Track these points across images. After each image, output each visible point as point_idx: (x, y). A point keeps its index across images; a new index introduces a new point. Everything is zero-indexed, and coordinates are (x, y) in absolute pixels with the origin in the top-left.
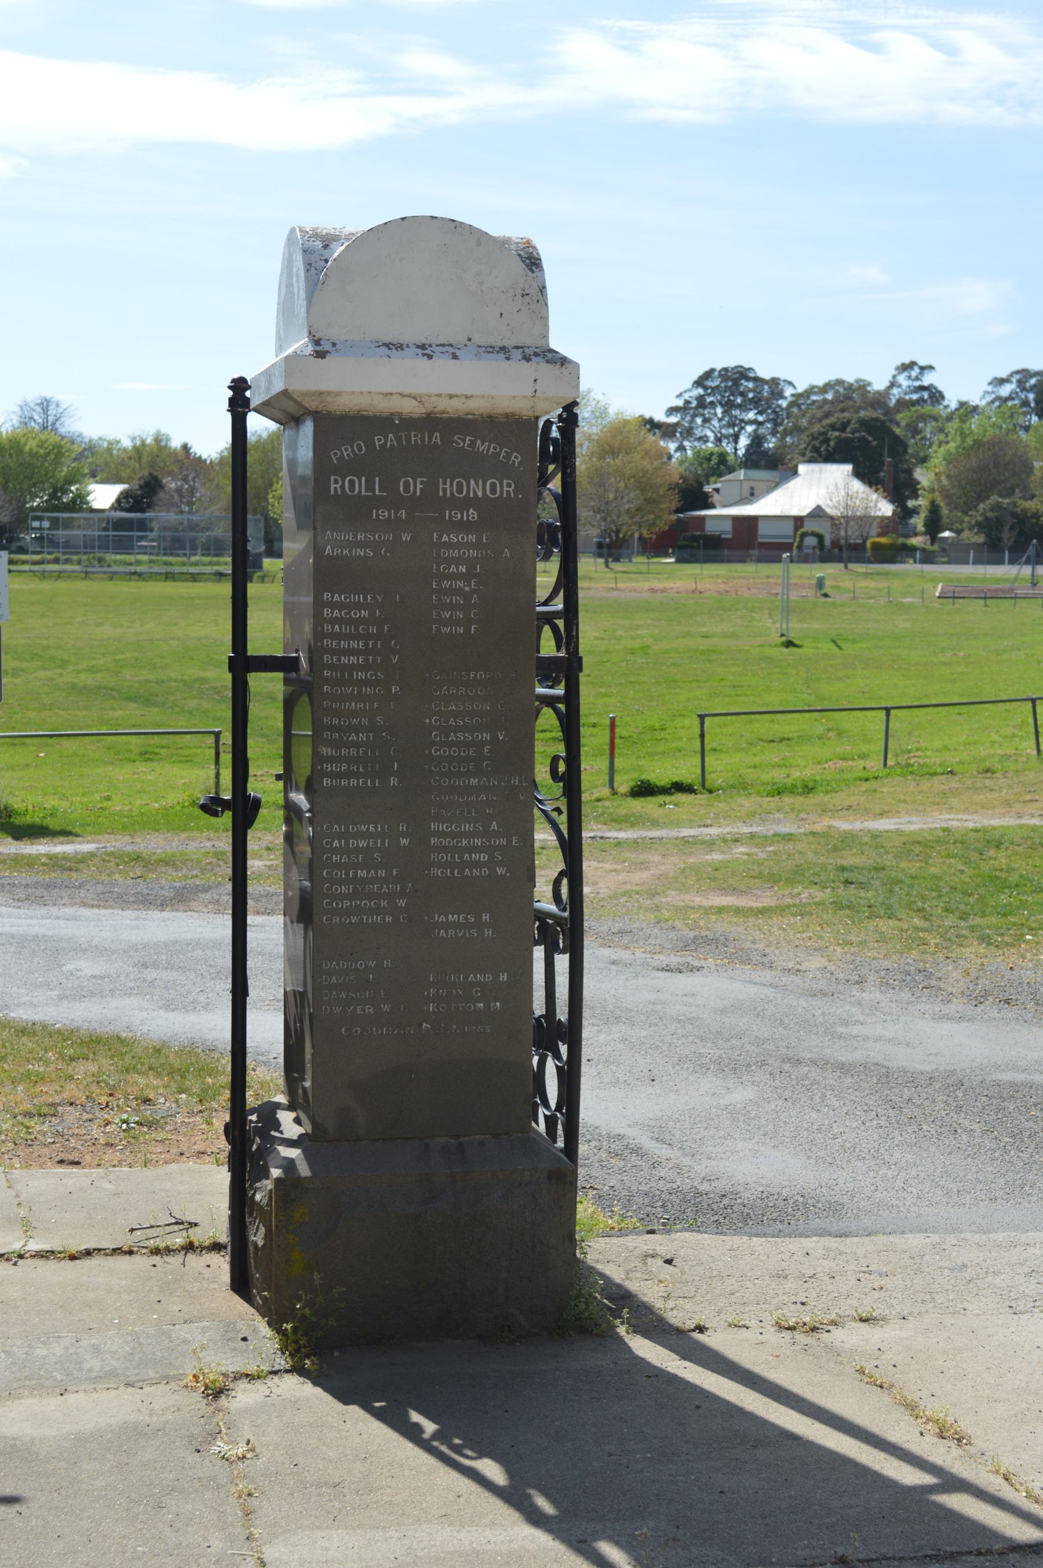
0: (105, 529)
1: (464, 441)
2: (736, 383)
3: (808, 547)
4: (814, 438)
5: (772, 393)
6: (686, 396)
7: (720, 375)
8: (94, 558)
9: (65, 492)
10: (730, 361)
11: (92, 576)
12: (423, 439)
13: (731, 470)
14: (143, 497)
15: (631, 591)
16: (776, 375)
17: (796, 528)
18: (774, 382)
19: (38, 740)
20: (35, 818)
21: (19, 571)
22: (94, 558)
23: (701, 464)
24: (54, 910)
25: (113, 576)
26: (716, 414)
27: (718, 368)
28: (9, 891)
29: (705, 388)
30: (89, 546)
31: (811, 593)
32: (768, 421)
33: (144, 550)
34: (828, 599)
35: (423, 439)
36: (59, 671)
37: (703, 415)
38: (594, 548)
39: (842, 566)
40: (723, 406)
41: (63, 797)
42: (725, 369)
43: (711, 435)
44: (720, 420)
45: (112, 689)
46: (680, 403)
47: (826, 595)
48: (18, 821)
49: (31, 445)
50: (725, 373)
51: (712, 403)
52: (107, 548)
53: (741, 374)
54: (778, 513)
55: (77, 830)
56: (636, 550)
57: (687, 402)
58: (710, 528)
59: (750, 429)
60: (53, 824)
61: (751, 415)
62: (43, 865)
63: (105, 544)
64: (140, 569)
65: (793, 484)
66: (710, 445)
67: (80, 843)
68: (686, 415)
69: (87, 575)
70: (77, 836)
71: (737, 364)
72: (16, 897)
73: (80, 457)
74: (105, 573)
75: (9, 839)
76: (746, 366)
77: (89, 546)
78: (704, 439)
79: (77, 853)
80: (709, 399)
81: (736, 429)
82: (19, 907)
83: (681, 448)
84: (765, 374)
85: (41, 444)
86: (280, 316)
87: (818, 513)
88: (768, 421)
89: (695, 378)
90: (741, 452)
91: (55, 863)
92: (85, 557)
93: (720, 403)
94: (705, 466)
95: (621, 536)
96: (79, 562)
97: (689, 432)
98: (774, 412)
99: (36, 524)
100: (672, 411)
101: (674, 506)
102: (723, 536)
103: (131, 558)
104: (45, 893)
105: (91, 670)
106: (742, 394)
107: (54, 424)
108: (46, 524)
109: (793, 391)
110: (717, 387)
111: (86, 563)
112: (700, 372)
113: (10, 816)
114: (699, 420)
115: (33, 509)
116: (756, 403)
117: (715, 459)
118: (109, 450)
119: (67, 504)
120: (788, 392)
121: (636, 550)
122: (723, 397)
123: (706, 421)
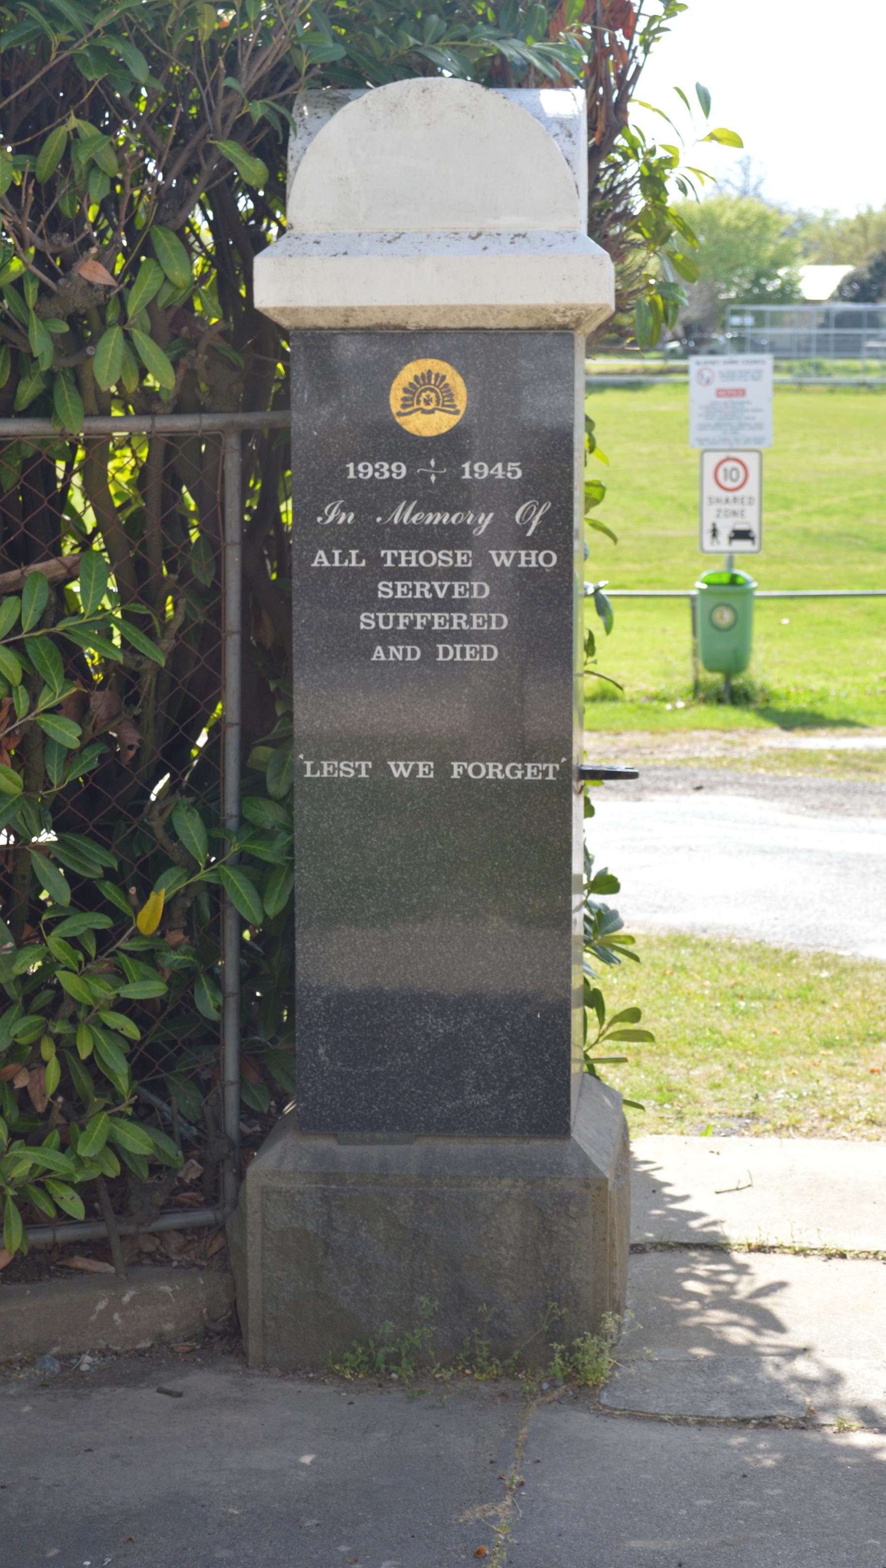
0: (822, 326)
8: (810, 364)
9: (772, 277)
11: (808, 388)
14: (871, 282)
19: (773, 603)
20: (800, 702)
22: (810, 364)
24: (862, 821)
25: (834, 388)
28: (798, 796)
30: (803, 348)
33: (875, 354)
36: (783, 513)
41: (829, 676)
45: (857, 537)
48: (782, 706)
49: (728, 217)
52: (827, 350)
55: (862, 719)
60: (831, 711)
62: (831, 763)
63: (823, 346)
64: (870, 378)
67: (870, 736)
69: (801, 387)
70: (864, 726)
72: (809, 804)
73: (791, 232)
74: (824, 384)
75: (776, 730)
77: (803, 348)
79: (871, 750)
82: (816, 817)
85: (741, 216)
91: (845, 761)
92: (796, 364)
96: (790, 370)
99: (736, 320)
103: (857, 364)
104: (845, 800)
105: (825, 512)
107: (756, 188)
108: (749, 320)
111: (798, 371)
113: (768, 701)
115: (730, 301)
118: (825, 221)
119: (775, 292)
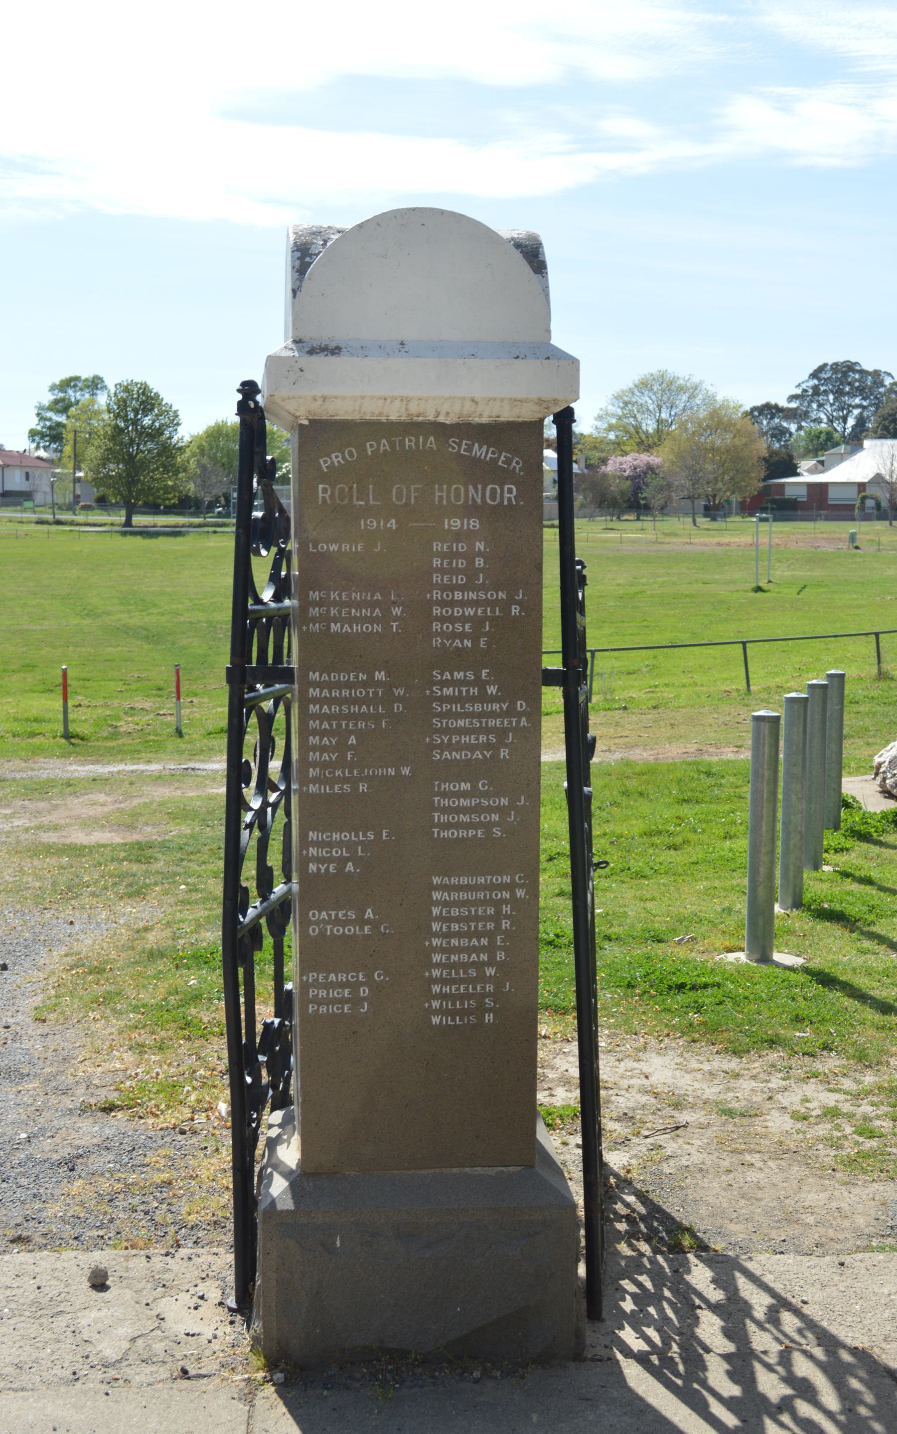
1: (460, 445)
2: (845, 375)
3: (869, 508)
4: (885, 419)
5: (875, 382)
6: (804, 386)
7: (832, 368)
10: (840, 357)
12: (417, 444)
13: (837, 444)
15: (701, 545)
16: (878, 368)
17: (859, 492)
18: (877, 373)
21: (223, 532)
23: (812, 441)
26: (828, 400)
27: (830, 363)
29: (819, 379)
31: (844, 546)
32: (870, 405)
34: (858, 551)
35: (417, 444)
37: (818, 401)
38: (702, 511)
39: (887, 523)
40: (834, 394)
42: (836, 364)
43: (823, 416)
44: (832, 405)
46: (799, 391)
47: (857, 548)
50: (835, 367)
51: (825, 391)
53: (849, 367)
54: (845, 481)
56: (734, 511)
57: (805, 391)
58: (789, 493)
59: (856, 412)
61: (857, 401)
65: (859, 457)
66: (823, 425)
68: (803, 401)
71: (845, 359)
76: (853, 361)
78: (818, 421)
80: (822, 388)
81: (845, 412)
83: (800, 428)
84: (869, 367)
86: (266, 380)
87: (878, 479)
88: (870, 405)
89: (811, 372)
90: (848, 431)
93: (832, 391)
94: (815, 442)
95: (717, 502)
97: (806, 415)
98: (876, 398)
100: (792, 398)
101: (762, 475)
102: (799, 499)
106: (849, 384)
109: (892, 381)
110: (829, 378)
112: (815, 366)
114: (815, 406)
116: (861, 391)
117: (823, 437)
120: (888, 381)
121: (734, 511)
122: (834, 386)
123: (820, 405)
